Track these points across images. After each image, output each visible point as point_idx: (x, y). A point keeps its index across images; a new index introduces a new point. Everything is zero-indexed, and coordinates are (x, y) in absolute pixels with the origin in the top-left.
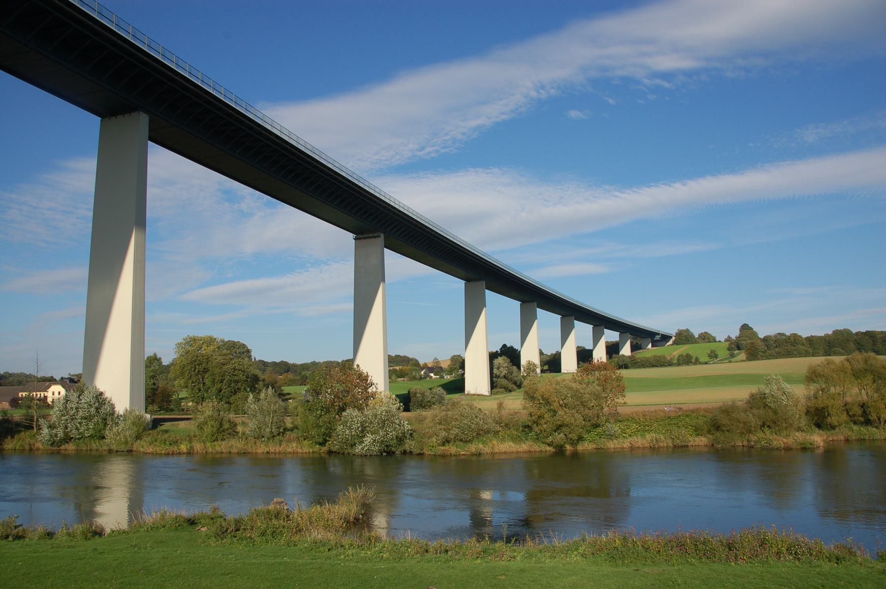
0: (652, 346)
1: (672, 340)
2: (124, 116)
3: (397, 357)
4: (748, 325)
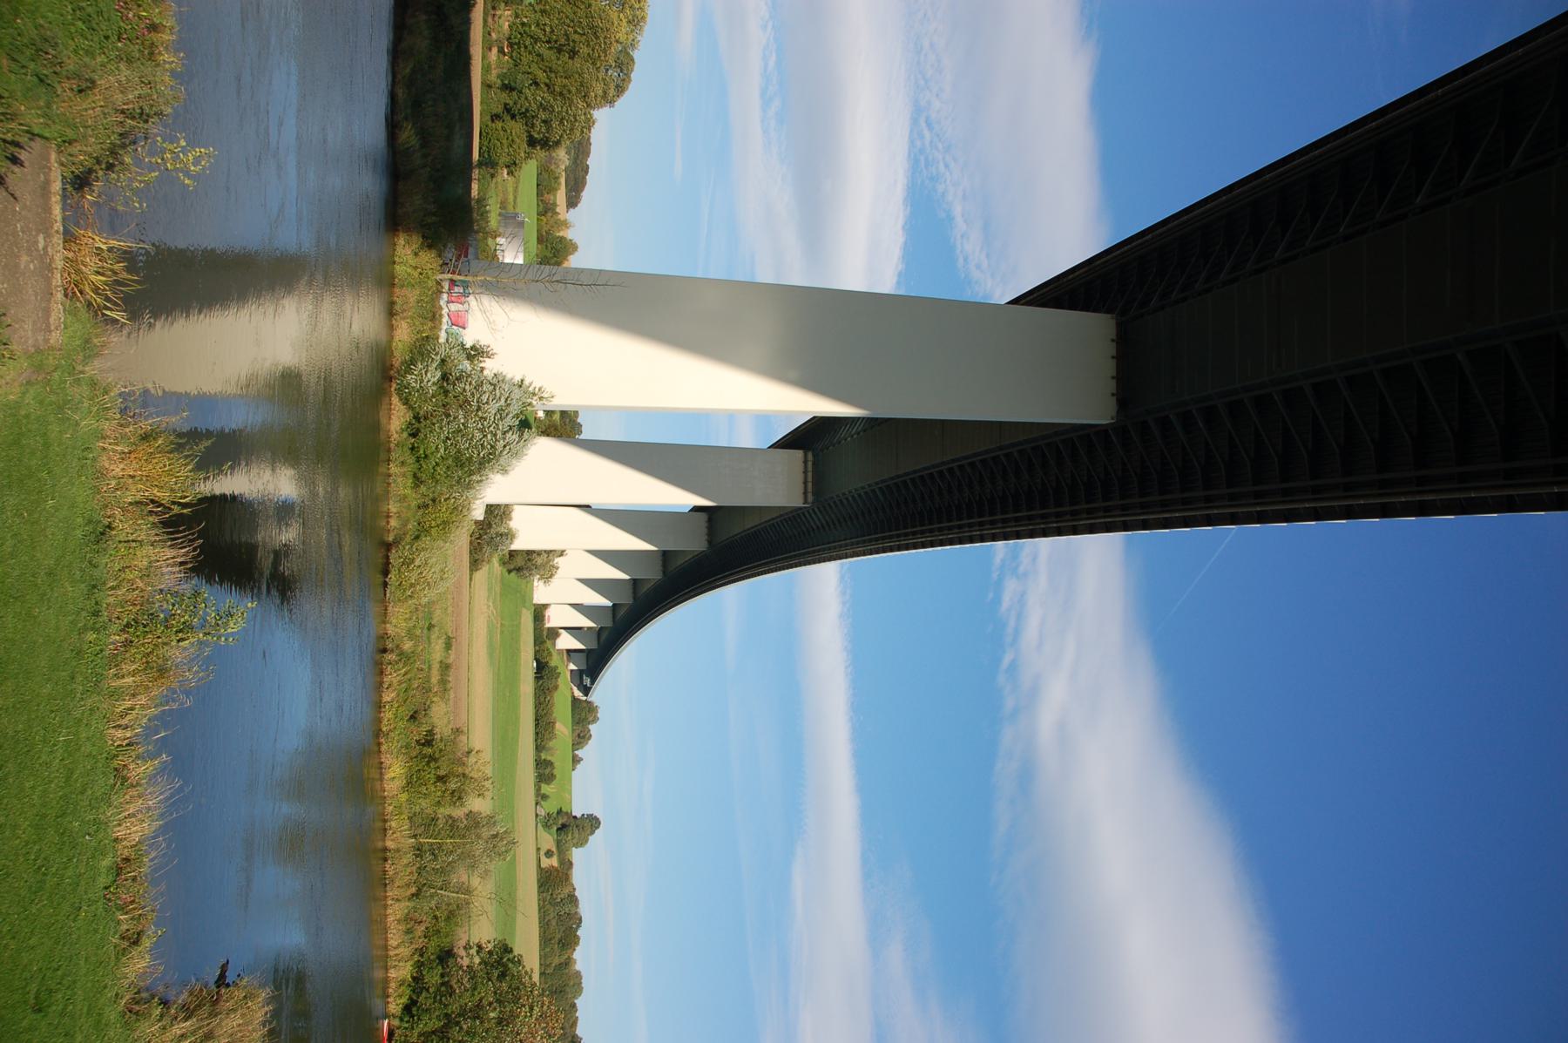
0: (572, 671)
1: (581, 694)
2: (1113, 378)
3: (585, 169)
4: (598, 827)
